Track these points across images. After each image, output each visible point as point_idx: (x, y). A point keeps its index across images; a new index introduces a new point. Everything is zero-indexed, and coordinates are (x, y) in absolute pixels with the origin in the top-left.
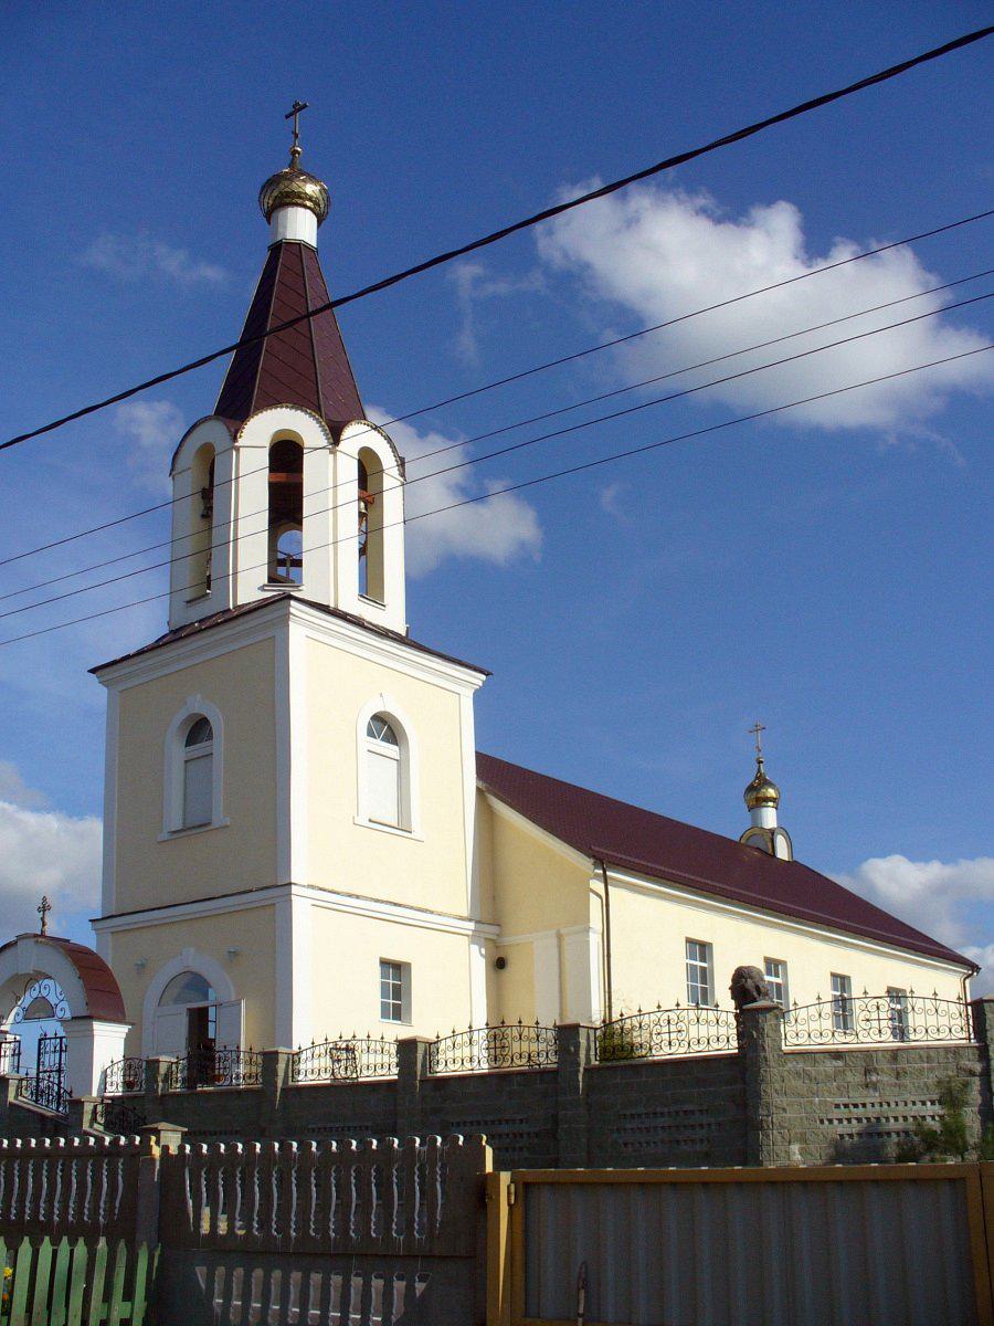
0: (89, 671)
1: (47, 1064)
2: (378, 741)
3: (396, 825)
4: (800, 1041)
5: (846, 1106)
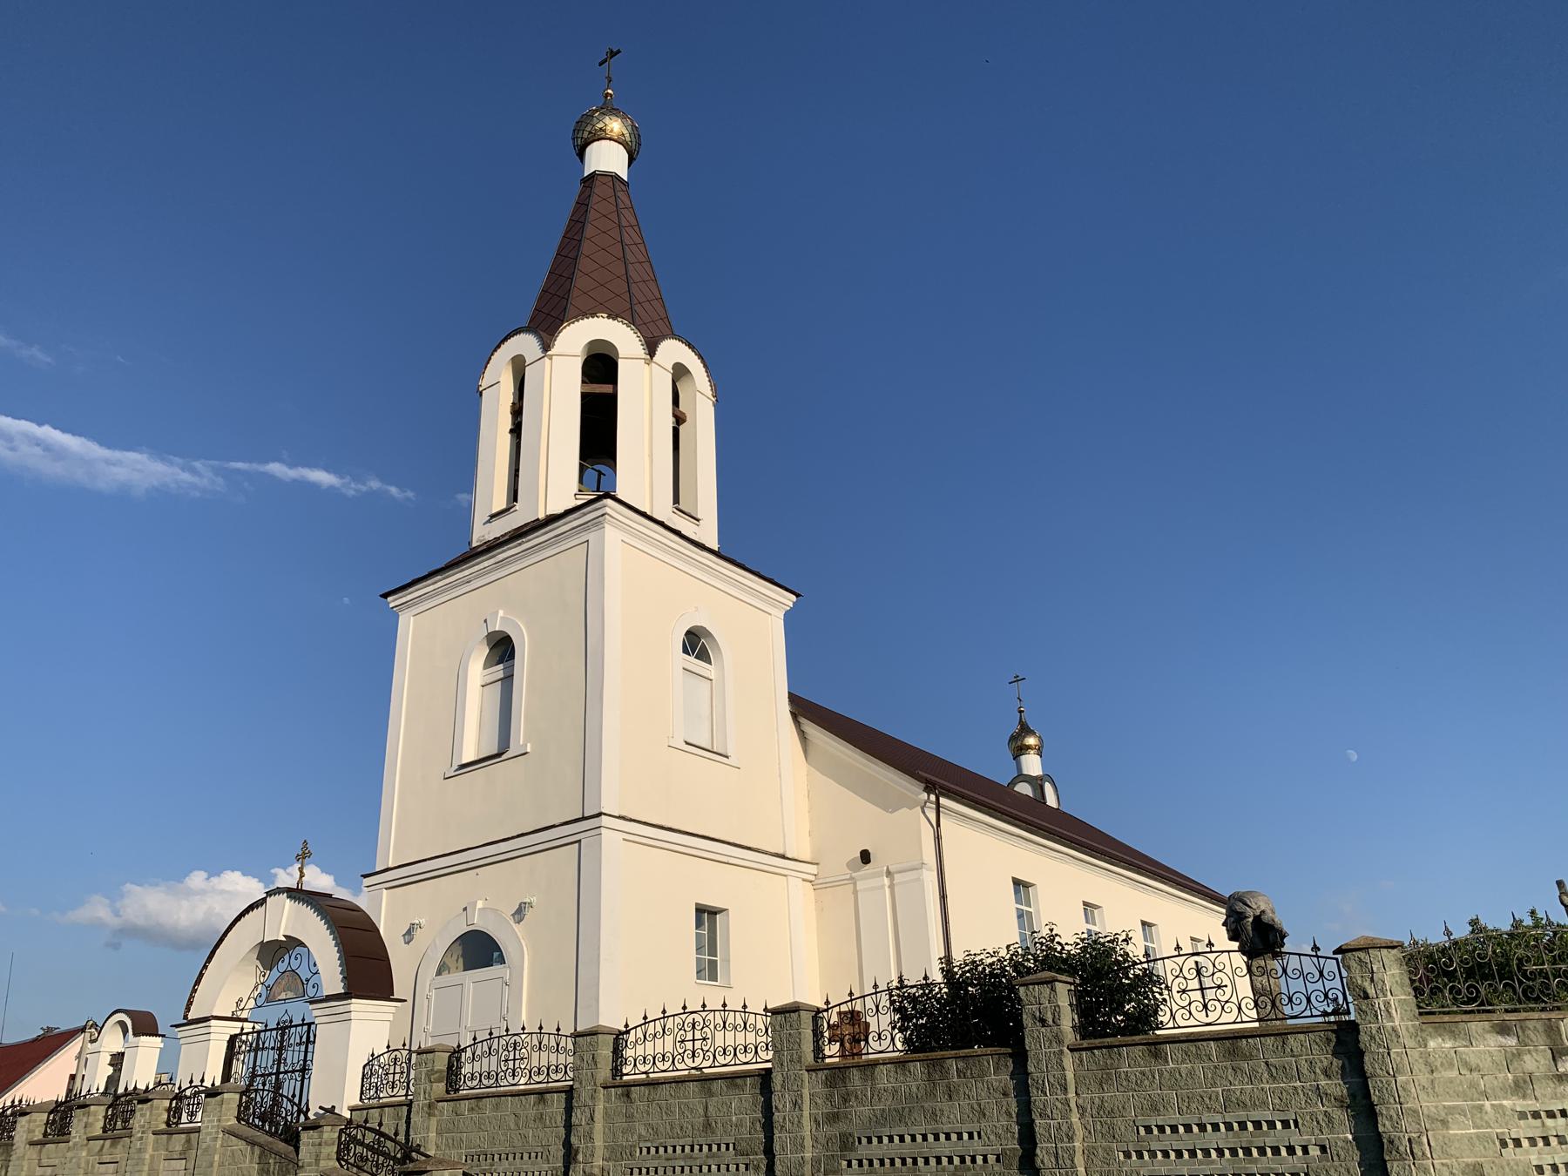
0: (381, 596)
1: (289, 1061)
2: (692, 658)
3: (710, 748)
4: (1212, 1017)
5: (1536, 1115)
